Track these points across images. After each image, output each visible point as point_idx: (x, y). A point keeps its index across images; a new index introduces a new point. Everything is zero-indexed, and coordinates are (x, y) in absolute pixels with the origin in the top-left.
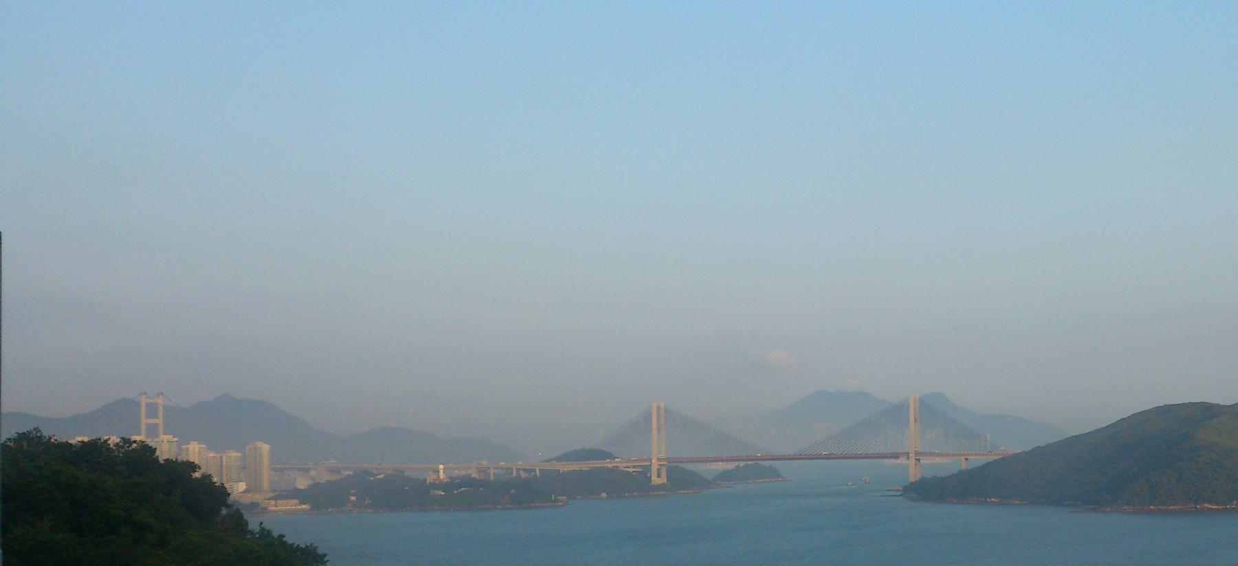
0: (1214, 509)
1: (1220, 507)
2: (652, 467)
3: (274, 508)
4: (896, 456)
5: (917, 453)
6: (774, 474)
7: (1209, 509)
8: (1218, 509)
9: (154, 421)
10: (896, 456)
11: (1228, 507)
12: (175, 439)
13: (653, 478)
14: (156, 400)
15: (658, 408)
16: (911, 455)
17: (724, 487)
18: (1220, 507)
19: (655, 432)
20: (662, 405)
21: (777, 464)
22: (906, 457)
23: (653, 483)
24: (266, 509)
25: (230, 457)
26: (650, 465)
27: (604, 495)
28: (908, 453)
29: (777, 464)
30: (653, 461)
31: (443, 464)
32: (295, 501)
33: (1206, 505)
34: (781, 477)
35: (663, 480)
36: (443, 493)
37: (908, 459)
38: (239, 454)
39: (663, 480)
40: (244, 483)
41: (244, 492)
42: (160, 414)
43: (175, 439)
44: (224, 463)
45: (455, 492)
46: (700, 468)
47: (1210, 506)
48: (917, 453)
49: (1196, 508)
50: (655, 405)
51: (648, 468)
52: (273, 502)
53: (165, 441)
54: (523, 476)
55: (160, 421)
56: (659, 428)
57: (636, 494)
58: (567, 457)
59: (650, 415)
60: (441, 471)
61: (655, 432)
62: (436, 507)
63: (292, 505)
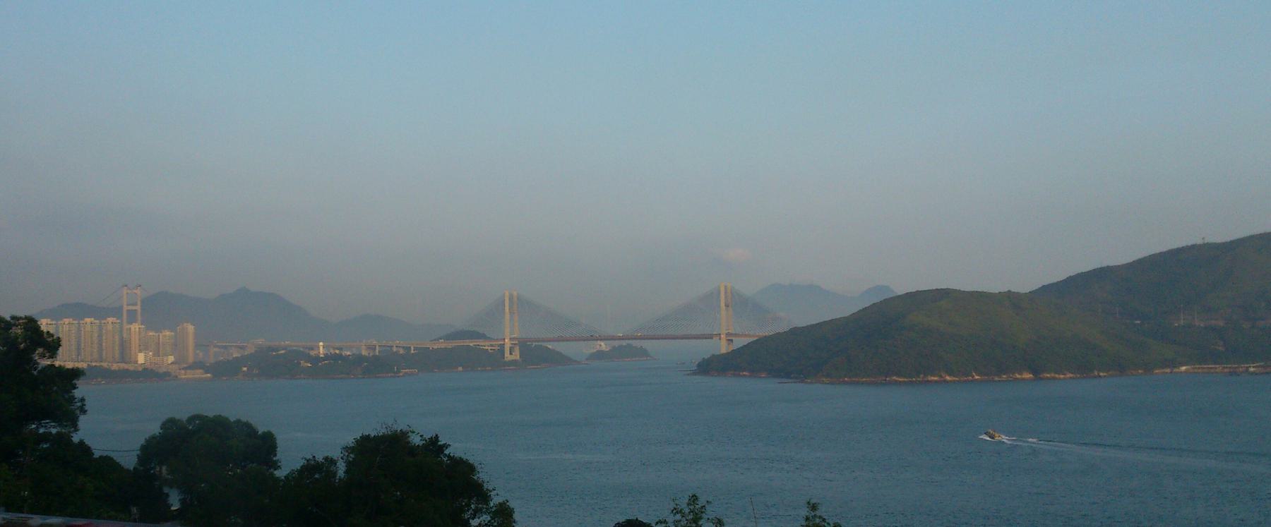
0: (900, 382)
1: (906, 380)
2: (506, 347)
3: (184, 376)
4: (710, 337)
5: (728, 334)
6: (643, 353)
7: (896, 381)
8: (954, 381)
9: (134, 308)
10: (710, 337)
11: (914, 379)
12: (118, 321)
13: (506, 356)
14: (135, 291)
15: (726, 287)
16: (722, 336)
17: (1212, 373)
18: (906, 380)
19: (507, 316)
20: (515, 294)
21: (647, 344)
22: (718, 338)
23: (506, 359)
24: (177, 377)
25: (165, 336)
26: (504, 344)
27: (460, 369)
28: (720, 334)
29: (647, 344)
30: (506, 340)
31: (323, 342)
32: (201, 371)
33: (894, 378)
34: (650, 357)
35: (516, 356)
36: (309, 365)
37: (720, 339)
38: (173, 333)
39: (516, 356)
40: (173, 357)
41: (172, 363)
42: (139, 303)
43: (118, 321)
44: (161, 339)
45: (320, 364)
46: (561, 347)
47: (897, 379)
48: (728, 334)
49: (886, 380)
50: (507, 294)
51: (502, 346)
52: (183, 372)
53: (110, 323)
54: (401, 353)
55: (138, 308)
56: (511, 313)
57: (490, 368)
58: (448, 337)
59: (719, 293)
60: (321, 348)
61: (507, 316)
62: (302, 376)
63: (199, 374)
